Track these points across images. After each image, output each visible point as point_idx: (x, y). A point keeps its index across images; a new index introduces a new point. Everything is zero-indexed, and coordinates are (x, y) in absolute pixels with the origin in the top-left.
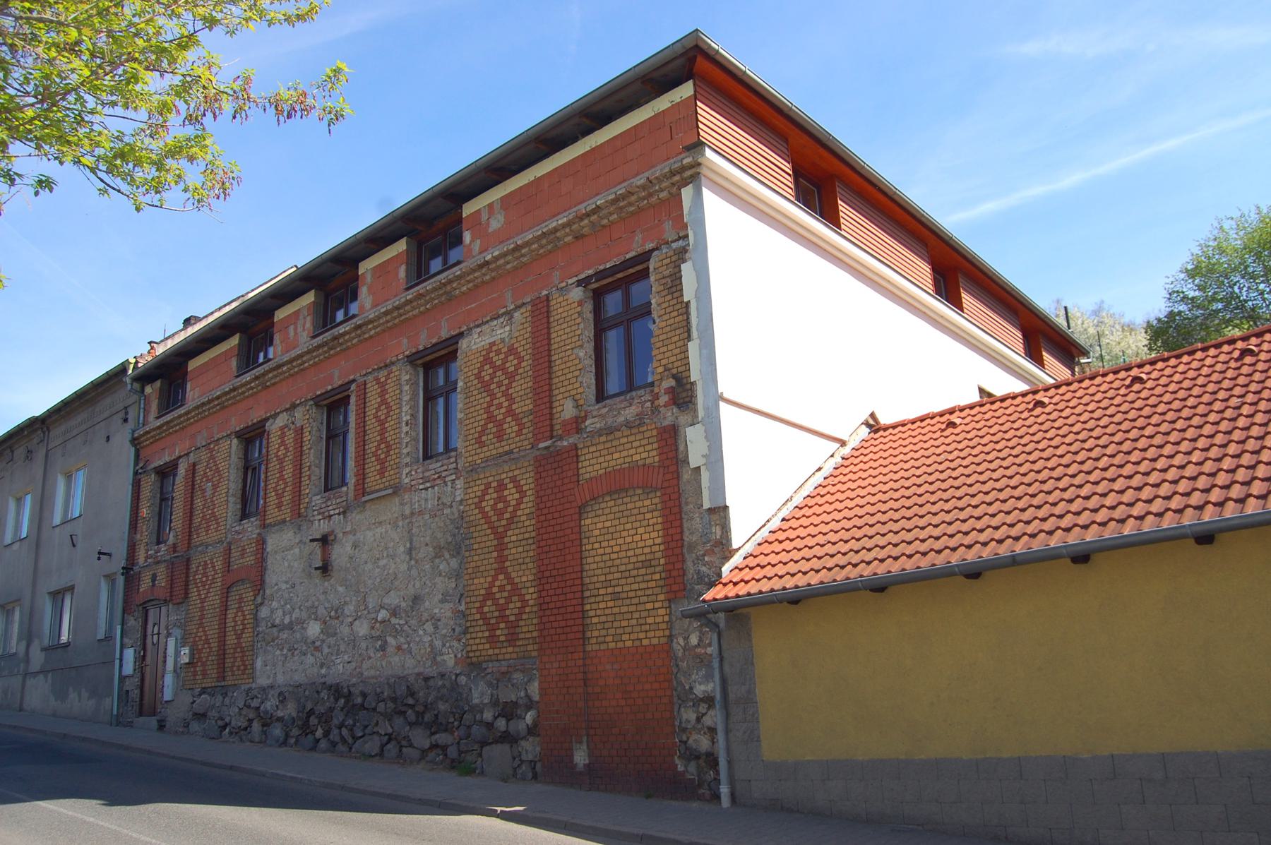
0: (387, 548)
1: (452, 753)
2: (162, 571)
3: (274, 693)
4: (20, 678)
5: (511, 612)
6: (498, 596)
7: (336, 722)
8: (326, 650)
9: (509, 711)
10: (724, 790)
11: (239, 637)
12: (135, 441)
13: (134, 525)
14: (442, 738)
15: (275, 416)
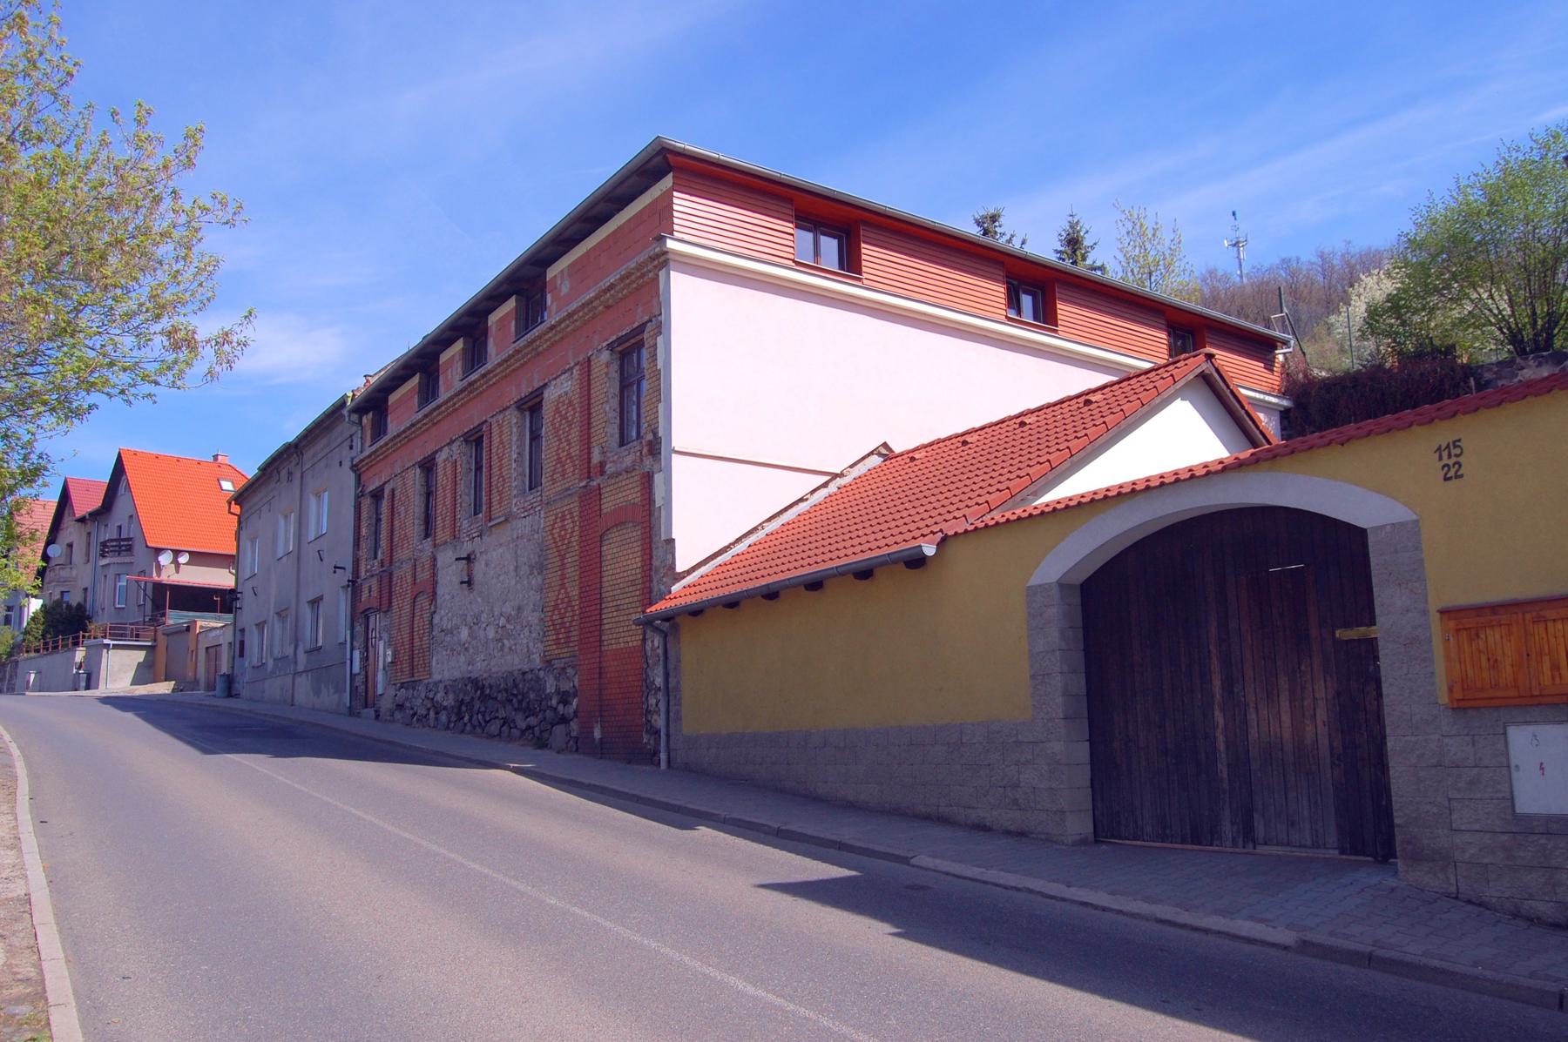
2: (374, 582)
3: (441, 686)
4: (289, 679)
9: (565, 699)
10: (663, 756)
12: (354, 468)
13: (357, 544)
15: (441, 449)
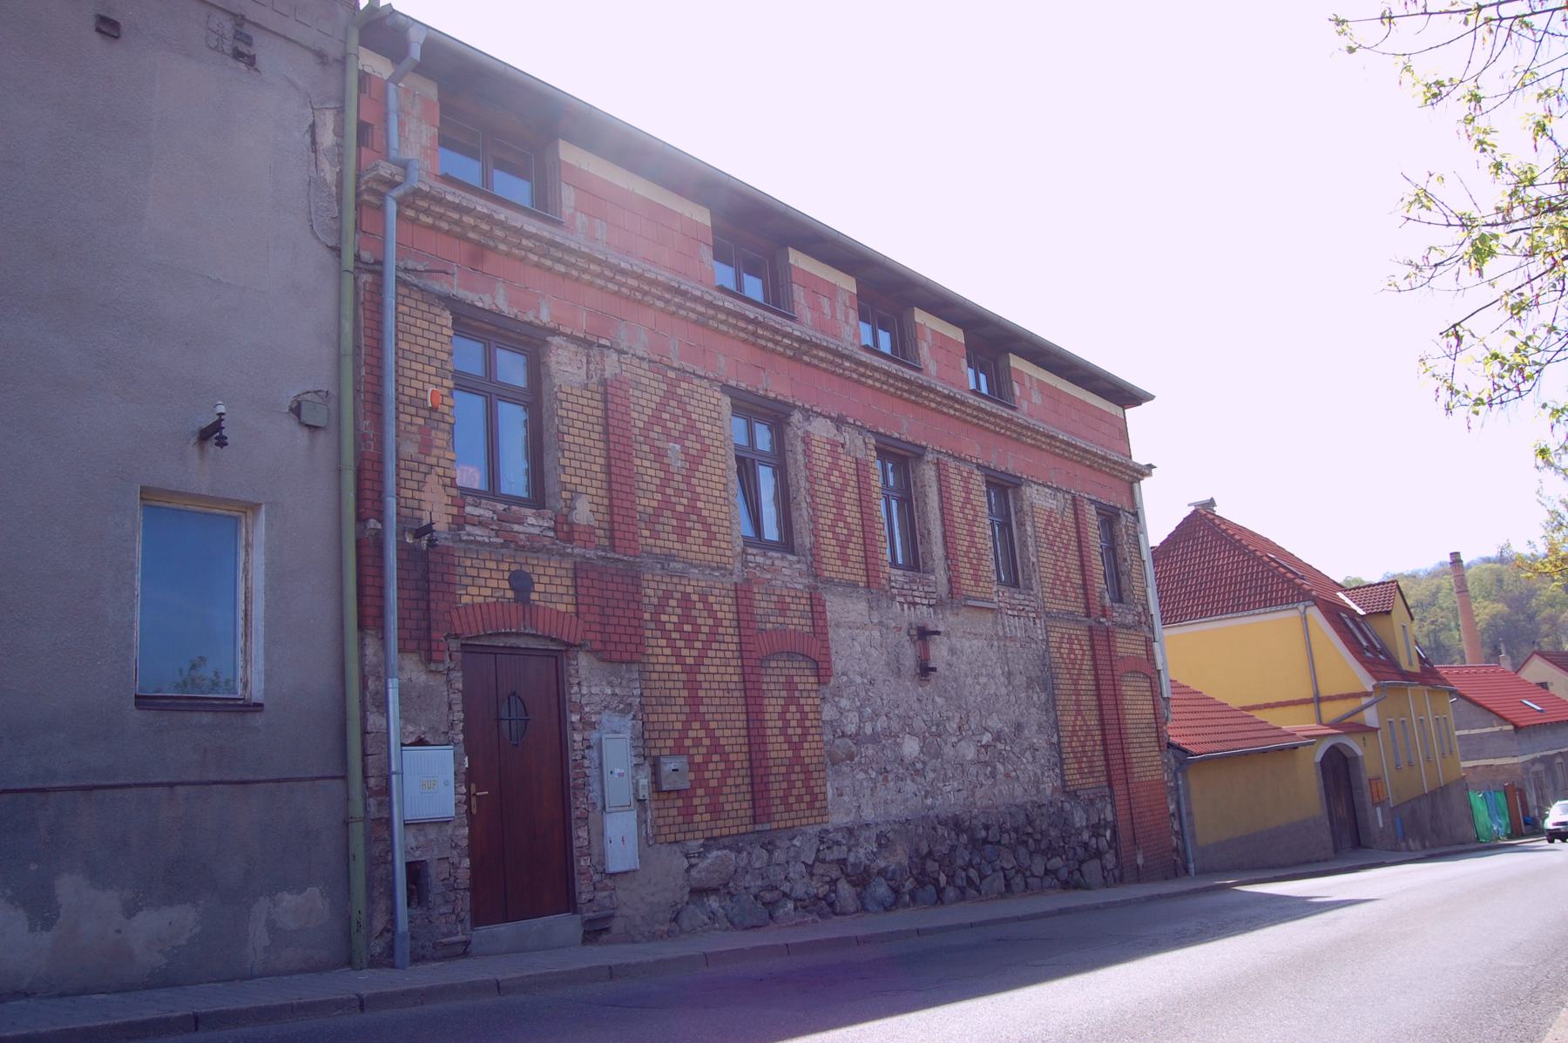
0: (984, 665)
1: (1064, 874)
5: (712, 776)
6: (693, 751)
7: (960, 862)
8: (931, 775)
11: (796, 747)
14: (1056, 862)
